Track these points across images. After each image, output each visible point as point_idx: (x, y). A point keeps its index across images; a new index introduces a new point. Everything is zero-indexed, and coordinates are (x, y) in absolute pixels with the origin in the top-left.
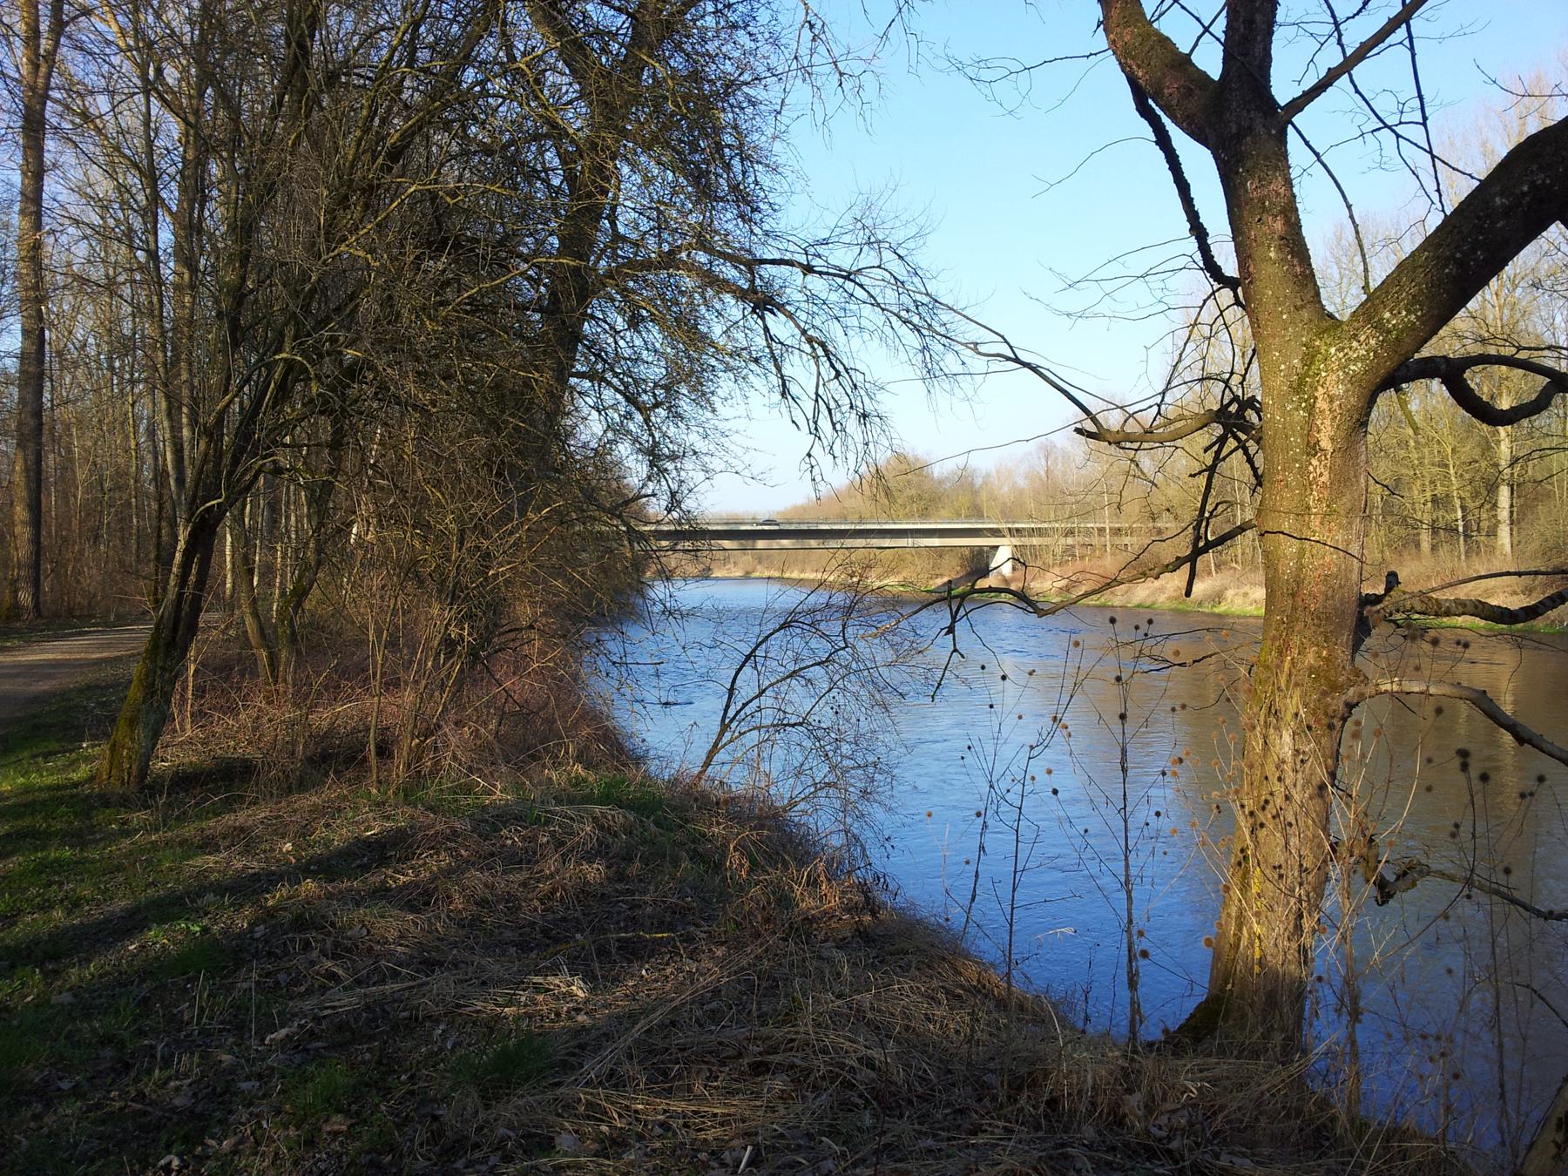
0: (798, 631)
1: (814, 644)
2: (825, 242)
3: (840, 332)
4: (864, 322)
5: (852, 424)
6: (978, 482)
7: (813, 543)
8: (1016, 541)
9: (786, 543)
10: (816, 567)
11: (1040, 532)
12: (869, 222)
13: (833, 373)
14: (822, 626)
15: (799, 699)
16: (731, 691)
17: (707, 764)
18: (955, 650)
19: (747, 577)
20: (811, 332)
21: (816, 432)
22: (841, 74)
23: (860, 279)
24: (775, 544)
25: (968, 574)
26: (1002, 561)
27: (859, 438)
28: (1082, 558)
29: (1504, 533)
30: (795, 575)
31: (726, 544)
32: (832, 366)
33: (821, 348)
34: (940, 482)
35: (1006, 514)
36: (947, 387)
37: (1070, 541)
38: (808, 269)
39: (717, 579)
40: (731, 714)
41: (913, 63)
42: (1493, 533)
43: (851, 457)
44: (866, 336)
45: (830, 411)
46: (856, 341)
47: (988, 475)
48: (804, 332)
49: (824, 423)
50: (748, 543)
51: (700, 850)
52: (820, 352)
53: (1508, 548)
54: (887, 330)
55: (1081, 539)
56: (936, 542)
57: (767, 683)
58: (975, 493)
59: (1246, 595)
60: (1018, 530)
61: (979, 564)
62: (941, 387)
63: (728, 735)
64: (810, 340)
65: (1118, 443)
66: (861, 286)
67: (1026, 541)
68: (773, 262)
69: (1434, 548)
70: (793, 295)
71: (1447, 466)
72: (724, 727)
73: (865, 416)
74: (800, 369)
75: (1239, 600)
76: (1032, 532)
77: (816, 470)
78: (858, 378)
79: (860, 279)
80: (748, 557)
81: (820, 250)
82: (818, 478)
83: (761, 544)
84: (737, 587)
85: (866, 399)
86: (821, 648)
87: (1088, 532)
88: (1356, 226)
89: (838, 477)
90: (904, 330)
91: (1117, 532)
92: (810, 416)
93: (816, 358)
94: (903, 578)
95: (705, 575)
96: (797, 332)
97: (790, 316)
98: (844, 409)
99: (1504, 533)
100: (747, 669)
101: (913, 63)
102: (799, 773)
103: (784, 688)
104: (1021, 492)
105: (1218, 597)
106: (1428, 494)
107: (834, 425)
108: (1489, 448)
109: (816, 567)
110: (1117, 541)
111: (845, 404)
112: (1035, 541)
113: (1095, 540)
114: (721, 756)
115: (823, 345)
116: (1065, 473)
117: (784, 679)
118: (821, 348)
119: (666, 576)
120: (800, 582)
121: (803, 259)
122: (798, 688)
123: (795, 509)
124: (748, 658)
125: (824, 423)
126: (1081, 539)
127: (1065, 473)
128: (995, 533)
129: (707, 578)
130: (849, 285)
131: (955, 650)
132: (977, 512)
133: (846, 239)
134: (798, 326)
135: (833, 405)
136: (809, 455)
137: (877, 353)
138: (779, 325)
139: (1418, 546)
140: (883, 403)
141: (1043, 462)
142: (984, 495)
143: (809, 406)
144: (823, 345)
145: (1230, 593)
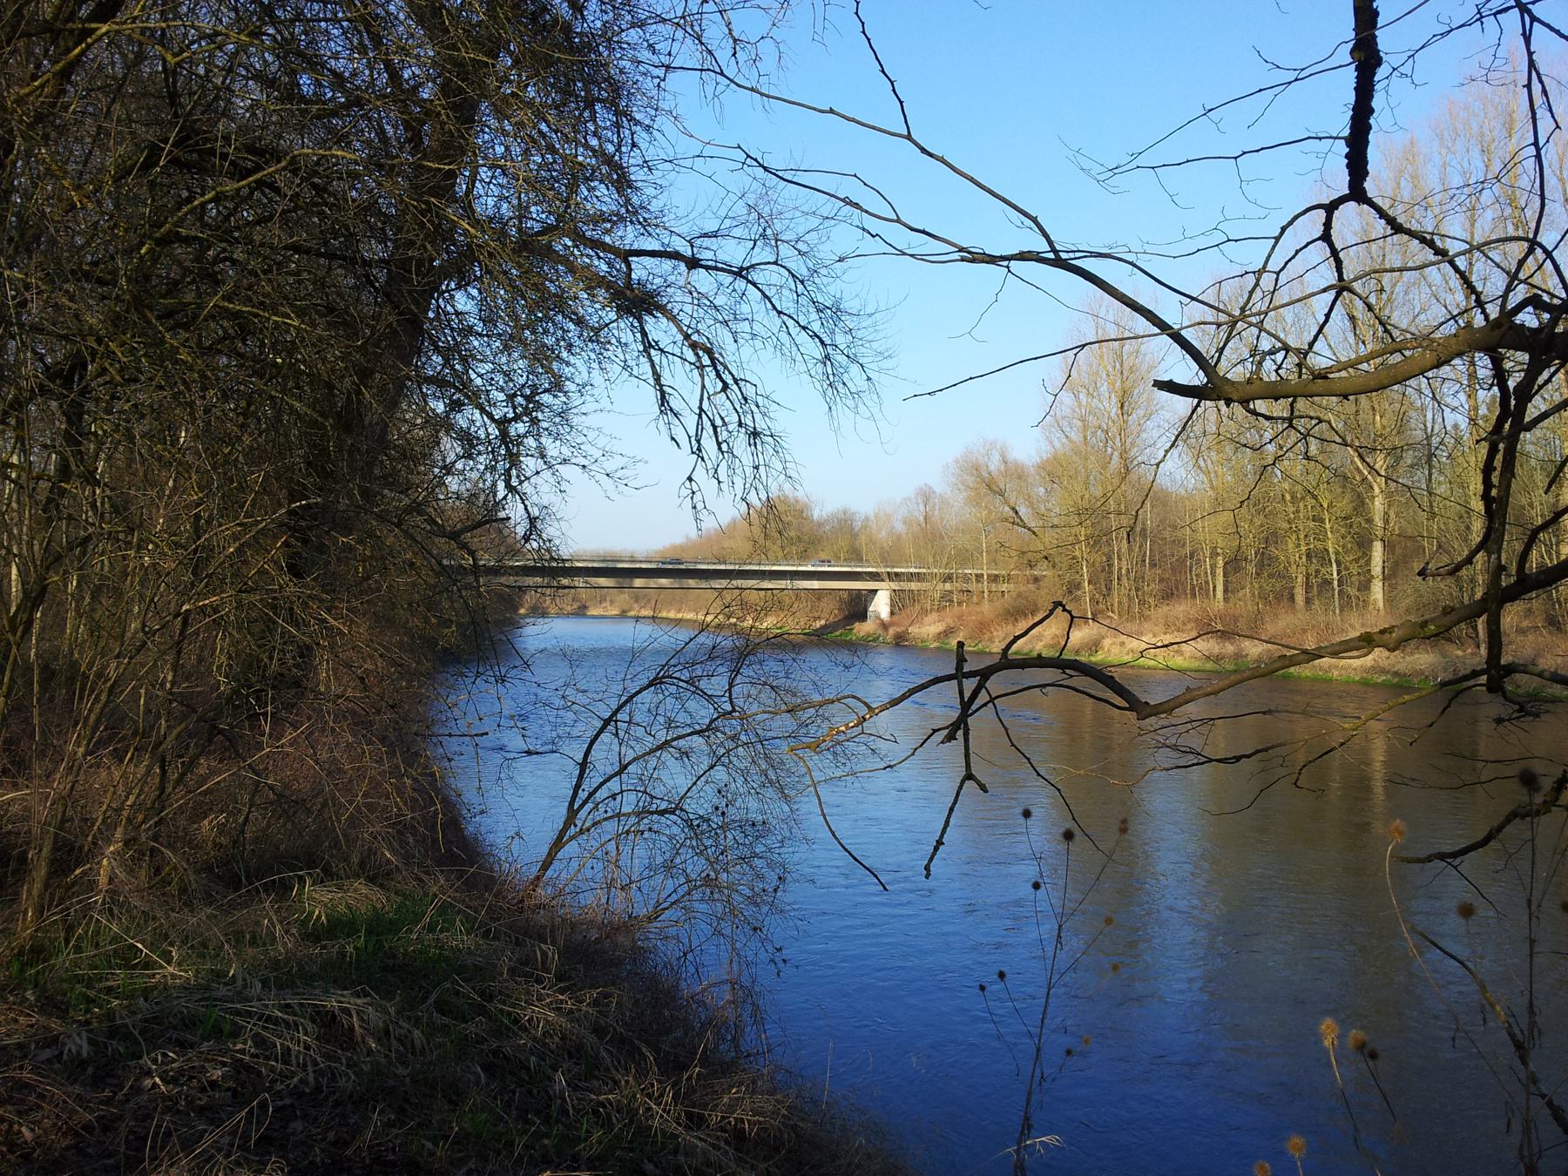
0: (673, 689)
1: (692, 705)
2: (715, 235)
3: (729, 338)
4: (757, 328)
5: (740, 443)
6: (858, 525)
7: (692, 583)
8: (894, 585)
9: (664, 582)
10: (695, 609)
11: (918, 577)
12: (766, 211)
13: (720, 385)
14: (703, 684)
15: (674, 777)
16: (583, 765)
17: (546, 865)
18: (969, 776)
19: (623, 615)
20: (695, 337)
21: (698, 451)
22: (735, 41)
23: (754, 276)
24: (653, 583)
25: (846, 618)
26: (881, 605)
27: (747, 460)
28: (960, 604)
29: (1377, 591)
30: (672, 615)
31: (603, 581)
32: (719, 376)
33: (706, 354)
34: (820, 525)
35: (885, 559)
36: (851, 403)
37: (948, 586)
38: (693, 263)
39: (594, 617)
40: (582, 795)
41: (819, 29)
42: (1365, 586)
43: (739, 482)
44: (758, 343)
45: (715, 428)
46: (746, 351)
47: (867, 519)
48: (687, 337)
49: (709, 443)
50: (626, 582)
51: (508, 1050)
52: (706, 361)
53: (1381, 604)
54: (784, 337)
55: (958, 585)
56: (816, 584)
57: (630, 755)
58: (854, 536)
59: (1123, 644)
60: (897, 574)
61: (857, 608)
62: (843, 413)
63: (572, 831)
64: (694, 346)
65: (1244, 402)
66: (754, 284)
67: (905, 585)
68: (653, 254)
69: (1308, 601)
70: (678, 300)
71: (1322, 521)
72: (572, 813)
73: (755, 434)
74: (683, 380)
75: (1116, 650)
76: (911, 577)
77: (698, 497)
78: (749, 391)
79: (754, 276)
80: (624, 597)
81: (706, 242)
82: (700, 506)
83: (638, 582)
84: (605, 627)
85: (758, 417)
86: (703, 713)
87: (966, 578)
88: (1297, 252)
89: (724, 509)
90: (803, 338)
91: (994, 579)
92: (692, 433)
93: (701, 367)
94: (773, 619)
95: (581, 612)
96: (680, 337)
97: (673, 318)
98: (730, 428)
99: (1377, 591)
100: (606, 737)
101: (819, 29)
102: (669, 867)
103: (653, 762)
104: (899, 538)
105: (1095, 646)
106: (1304, 548)
107: (719, 444)
108: (1363, 503)
109: (695, 609)
110: (994, 587)
111: (730, 423)
112: (914, 586)
113: (973, 586)
114: (571, 849)
115: (709, 352)
116: (942, 519)
117: (652, 751)
118: (706, 354)
119: (539, 612)
120: (678, 622)
121: (687, 251)
122: (671, 762)
123: (674, 548)
124: (607, 722)
125: (709, 443)
126: (958, 585)
127: (942, 519)
128: (875, 577)
129: (584, 616)
130: (741, 284)
131: (969, 776)
132: (856, 555)
133: (737, 232)
134: (681, 330)
135: (718, 422)
136: (690, 479)
137: (773, 369)
138: (658, 328)
139: (1292, 598)
140: (780, 421)
141: (922, 507)
142: (863, 538)
143: (691, 421)
144: (709, 352)
145: (1107, 642)
